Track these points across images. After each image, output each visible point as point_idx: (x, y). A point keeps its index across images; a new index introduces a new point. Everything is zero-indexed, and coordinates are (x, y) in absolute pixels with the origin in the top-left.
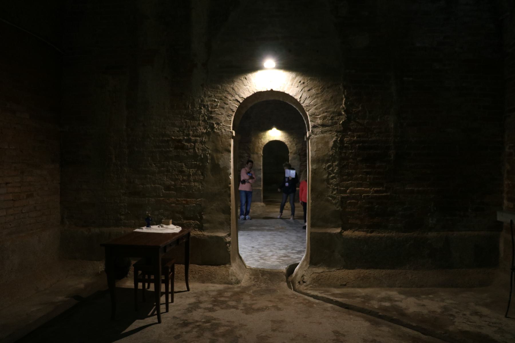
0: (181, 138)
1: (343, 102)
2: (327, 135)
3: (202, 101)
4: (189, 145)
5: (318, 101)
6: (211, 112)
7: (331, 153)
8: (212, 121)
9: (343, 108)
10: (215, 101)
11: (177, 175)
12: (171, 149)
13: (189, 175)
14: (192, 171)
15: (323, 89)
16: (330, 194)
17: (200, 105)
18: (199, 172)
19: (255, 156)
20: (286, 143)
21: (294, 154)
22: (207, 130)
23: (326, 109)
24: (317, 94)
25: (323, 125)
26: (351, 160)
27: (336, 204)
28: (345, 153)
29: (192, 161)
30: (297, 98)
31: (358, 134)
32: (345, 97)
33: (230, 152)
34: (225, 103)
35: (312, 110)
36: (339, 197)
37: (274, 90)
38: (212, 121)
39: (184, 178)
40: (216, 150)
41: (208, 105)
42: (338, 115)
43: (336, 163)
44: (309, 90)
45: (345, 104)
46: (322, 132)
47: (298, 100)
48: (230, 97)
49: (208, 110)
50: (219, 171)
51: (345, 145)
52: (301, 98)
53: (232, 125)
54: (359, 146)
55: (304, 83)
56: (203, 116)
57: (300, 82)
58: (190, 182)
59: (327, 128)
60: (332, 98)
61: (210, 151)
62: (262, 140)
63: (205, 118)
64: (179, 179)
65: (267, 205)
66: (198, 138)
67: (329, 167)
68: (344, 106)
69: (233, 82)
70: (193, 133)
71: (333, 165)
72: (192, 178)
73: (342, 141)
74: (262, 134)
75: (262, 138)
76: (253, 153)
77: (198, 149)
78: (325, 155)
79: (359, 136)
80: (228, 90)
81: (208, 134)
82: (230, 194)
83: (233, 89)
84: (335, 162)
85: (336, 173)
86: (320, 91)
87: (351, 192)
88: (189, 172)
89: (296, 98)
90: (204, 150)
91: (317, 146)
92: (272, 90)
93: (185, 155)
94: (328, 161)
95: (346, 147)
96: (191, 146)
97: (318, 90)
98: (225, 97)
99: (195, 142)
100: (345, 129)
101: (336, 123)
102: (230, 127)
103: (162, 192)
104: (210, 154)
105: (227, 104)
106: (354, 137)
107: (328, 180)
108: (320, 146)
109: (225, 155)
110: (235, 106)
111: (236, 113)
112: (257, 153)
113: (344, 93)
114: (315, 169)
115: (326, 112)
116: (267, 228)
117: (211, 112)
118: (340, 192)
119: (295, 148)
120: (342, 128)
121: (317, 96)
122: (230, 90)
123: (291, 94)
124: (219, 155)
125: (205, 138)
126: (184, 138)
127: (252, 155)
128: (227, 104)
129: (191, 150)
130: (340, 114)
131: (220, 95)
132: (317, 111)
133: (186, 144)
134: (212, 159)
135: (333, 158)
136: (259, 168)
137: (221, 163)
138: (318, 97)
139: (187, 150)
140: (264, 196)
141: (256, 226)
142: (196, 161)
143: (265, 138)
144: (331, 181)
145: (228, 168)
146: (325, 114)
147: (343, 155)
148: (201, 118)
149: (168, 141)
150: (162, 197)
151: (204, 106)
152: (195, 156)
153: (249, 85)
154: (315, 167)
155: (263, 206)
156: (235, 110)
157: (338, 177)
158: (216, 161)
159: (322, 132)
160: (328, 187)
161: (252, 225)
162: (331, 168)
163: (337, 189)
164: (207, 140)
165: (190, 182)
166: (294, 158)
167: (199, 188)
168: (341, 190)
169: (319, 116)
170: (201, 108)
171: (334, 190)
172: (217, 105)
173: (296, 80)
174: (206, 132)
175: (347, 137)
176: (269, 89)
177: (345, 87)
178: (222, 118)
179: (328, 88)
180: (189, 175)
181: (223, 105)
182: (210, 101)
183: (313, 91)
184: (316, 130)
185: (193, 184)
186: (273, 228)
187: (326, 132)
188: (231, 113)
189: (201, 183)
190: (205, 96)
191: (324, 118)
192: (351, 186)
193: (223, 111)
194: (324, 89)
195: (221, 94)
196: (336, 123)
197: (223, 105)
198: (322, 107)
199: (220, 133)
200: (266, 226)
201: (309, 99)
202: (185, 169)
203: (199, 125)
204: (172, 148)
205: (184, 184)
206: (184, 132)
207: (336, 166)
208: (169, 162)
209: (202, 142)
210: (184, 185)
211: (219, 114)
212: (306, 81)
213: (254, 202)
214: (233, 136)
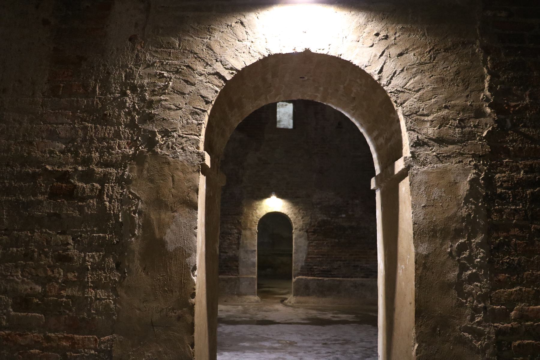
0: (69, 168)
1: (486, 85)
2: (452, 165)
3: (129, 76)
4: (87, 187)
5: (426, 81)
6: (150, 105)
7: (464, 212)
8: (150, 127)
9: (487, 100)
10: (162, 76)
11: (52, 268)
12: (40, 198)
13: (83, 270)
14: (92, 258)
15: (435, 52)
16: (466, 323)
17: (124, 84)
18: (111, 262)
19: (248, 233)
20: (289, 216)
21: (300, 231)
22: (137, 149)
23: (446, 100)
24: (421, 64)
25: (440, 141)
26: (515, 231)
27: (483, 350)
28: (500, 212)
29: (93, 232)
30: (373, 71)
31: (528, 163)
32: (489, 73)
33: (196, 209)
34: (187, 82)
35: (412, 102)
36: (489, 330)
37: (313, 50)
38: (150, 127)
39: (70, 276)
40: (159, 203)
41: (142, 86)
42: (476, 117)
43: (479, 240)
44: (401, 55)
45: (490, 89)
46: (440, 158)
47: (376, 78)
48: (199, 67)
49: (143, 99)
50: (166, 259)
51: (499, 190)
52: (381, 71)
53: (202, 138)
54: (532, 193)
55: (386, 37)
56: (129, 114)
57: (377, 35)
58: (84, 286)
59: (450, 147)
60: (457, 73)
61: (140, 206)
62: (258, 211)
63: (133, 118)
64: (56, 280)
65: (262, 298)
66: (113, 171)
67: (462, 248)
68: (488, 93)
69: (210, 31)
70: (101, 157)
71: (471, 243)
72: (89, 277)
73: (489, 181)
74: (257, 203)
75: (257, 208)
76: (245, 229)
77: (111, 198)
78: (450, 218)
79: (530, 169)
80: (196, 50)
81: (138, 159)
82: (193, 324)
83: (209, 47)
84: (475, 237)
85: (480, 267)
86: (427, 57)
87: (522, 317)
88: (84, 260)
89: (368, 70)
90: (124, 201)
91: (428, 195)
92: (307, 51)
93: (77, 214)
94: (458, 233)
95: (500, 196)
96: (92, 190)
97: (422, 54)
98: (188, 66)
99: (104, 179)
100: (494, 153)
101: (472, 136)
102: (198, 141)
103: (8, 314)
104: (140, 213)
105: (193, 84)
106: (518, 170)
107: (459, 285)
108: (436, 193)
109: (182, 215)
110: (212, 91)
111: (214, 107)
112: (250, 229)
113: (485, 63)
114: (427, 256)
115: (446, 107)
116: (267, 344)
117: (150, 105)
118: (493, 316)
119: (301, 223)
120: (488, 149)
121: (420, 68)
122: (199, 48)
123: (356, 62)
124: (165, 216)
125: (131, 171)
126: (76, 169)
127: (243, 232)
128: (193, 84)
129: (93, 202)
130: (479, 113)
131: (176, 62)
132: (422, 105)
133: (80, 184)
134: (147, 225)
135: (468, 227)
136: (253, 249)
137: (169, 236)
138: (423, 72)
139: (83, 199)
140: (258, 284)
141: (249, 340)
142: (105, 232)
143: (261, 208)
144: (469, 287)
145: (186, 252)
146: (445, 112)
147: (495, 217)
148: (123, 119)
149: (34, 176)
150: (5, 328)
151: (134, 89)
152: (102, 217)
153: (251, 38)
154: (424, 249)
155: (257, 302)
156: (212, 97)
157: (485, 274)
158: (157, 231)
159: (440, 158)
160: (462, 305)
161: (244, 339)
162: (467, 253)
163: (485, 308)
164: (134, 174)
165: (84, 286)
166: (300, 236)
167: (107, 305)
168: (494, 309)
169: (430, 118)
170: (124, 94)
171: (476, 310)
172: (166, 87)
173: (367, 30)
174: (134, 154)
175: (502, 172)
176: (300, 49)
177: (487, 50)
178: (177, 119)
179: (446, 50)
180: (83, 270)
181: (181, 85)
182: (149, 75)
183: (411, 57)
184: (422, 152)
185: (91, 293)
186: (277, 345)
187: (449, 156)
188: (201, 105)
189: (114, 290)
190: (137, 65)
191: (443, 122)
192: (522, 301)
193: (179, 101)
194: (437, 52)
195: (177, 58)
196: (472, 136)
197: (181, 85)
198: (435, 95)
199: (170, 159)
200: (266, 340)
201: (402, 75)
202: (73, 252)
203: (117, 135)
204: (43, 194)
205: (69, 292)
206: (77, 154)
207: (479, 245)
208: (33, 232)
209: (122, 181)
210: (68, 297)
211: (170, 109)
212: (391, 34)
213: (246, 295)
214: (204, 166)
